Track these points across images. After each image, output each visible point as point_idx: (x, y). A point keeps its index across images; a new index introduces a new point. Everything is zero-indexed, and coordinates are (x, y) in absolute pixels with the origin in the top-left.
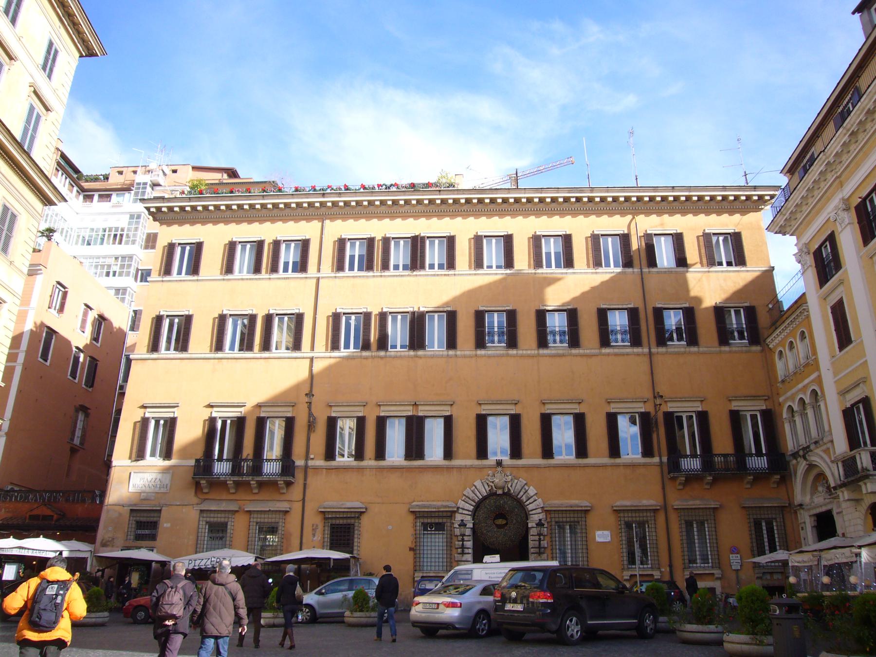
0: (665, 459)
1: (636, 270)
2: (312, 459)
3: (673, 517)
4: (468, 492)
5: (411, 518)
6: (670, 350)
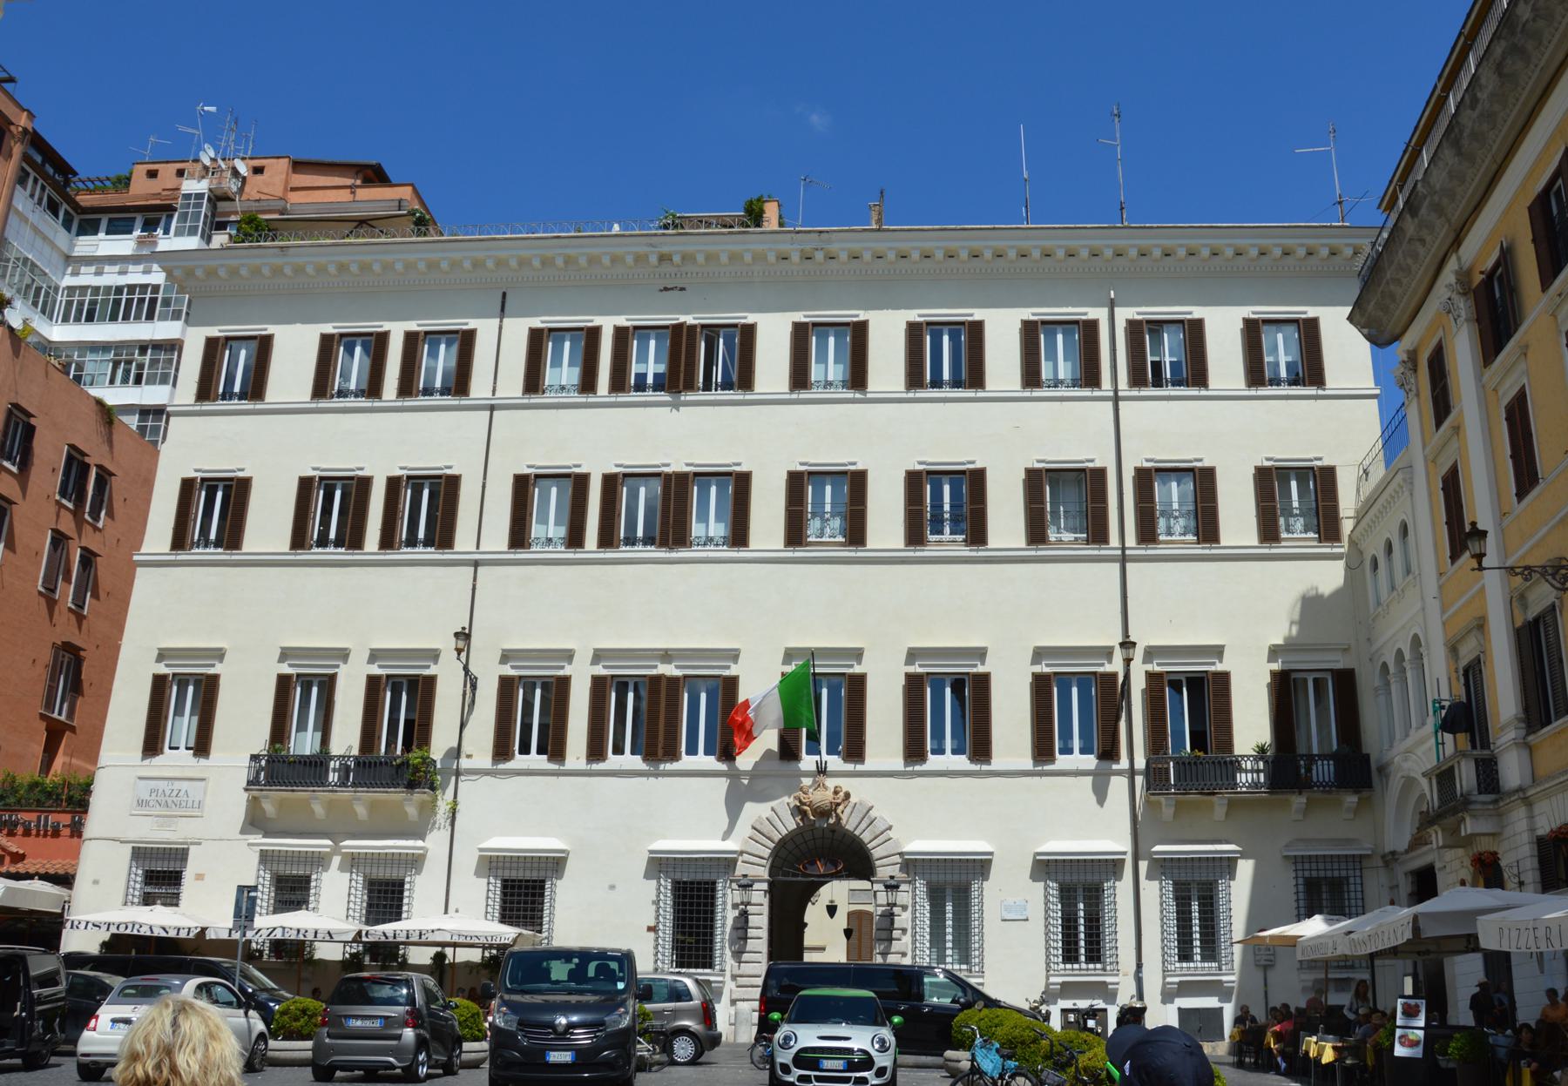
2: (469, 756)
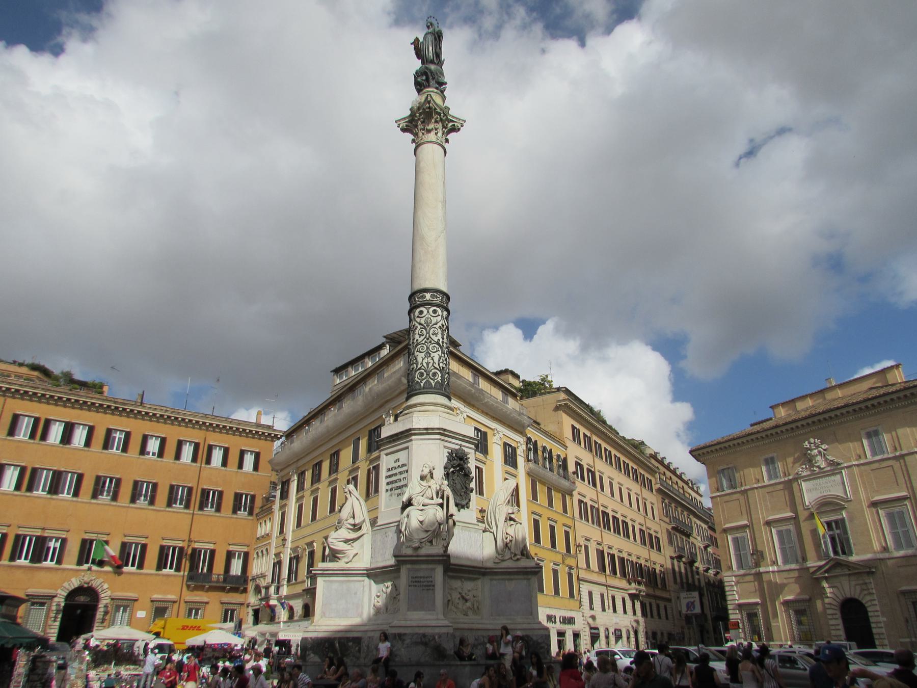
0: (186, 573)
1: (198, 465)
3: (183, 605)
4: (66, 584)
5: (150, 603)
6: (205, 513)
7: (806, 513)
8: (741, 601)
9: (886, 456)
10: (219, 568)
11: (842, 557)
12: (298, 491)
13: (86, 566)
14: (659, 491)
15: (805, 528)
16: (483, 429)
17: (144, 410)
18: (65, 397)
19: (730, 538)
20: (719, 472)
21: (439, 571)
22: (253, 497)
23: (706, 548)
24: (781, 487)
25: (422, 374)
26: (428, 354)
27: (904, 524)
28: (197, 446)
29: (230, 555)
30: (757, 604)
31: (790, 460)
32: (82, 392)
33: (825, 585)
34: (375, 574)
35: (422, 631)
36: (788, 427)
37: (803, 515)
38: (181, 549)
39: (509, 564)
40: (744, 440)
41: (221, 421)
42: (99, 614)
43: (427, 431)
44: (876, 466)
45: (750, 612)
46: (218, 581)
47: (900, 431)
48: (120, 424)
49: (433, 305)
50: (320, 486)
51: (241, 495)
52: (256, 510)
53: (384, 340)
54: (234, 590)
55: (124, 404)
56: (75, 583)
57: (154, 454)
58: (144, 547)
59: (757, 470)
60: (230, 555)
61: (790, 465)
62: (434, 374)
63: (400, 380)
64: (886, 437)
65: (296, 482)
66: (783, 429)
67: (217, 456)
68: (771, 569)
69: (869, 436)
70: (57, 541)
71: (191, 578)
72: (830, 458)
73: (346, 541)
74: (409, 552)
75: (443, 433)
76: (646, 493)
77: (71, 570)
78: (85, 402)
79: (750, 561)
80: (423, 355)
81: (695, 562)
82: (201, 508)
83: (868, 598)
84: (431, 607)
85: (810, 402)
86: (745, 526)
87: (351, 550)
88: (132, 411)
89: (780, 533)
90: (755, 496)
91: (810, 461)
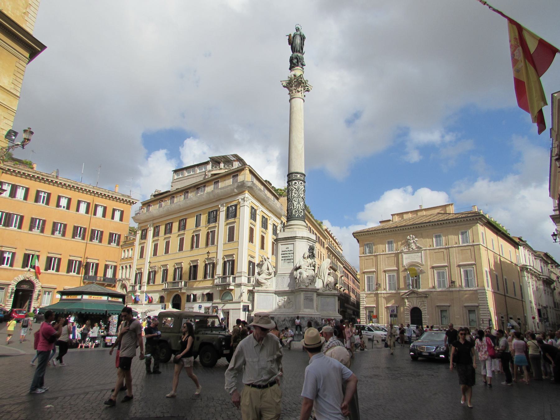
4: (16, 278)
7: (403, 269)
8: (367, 305)
9: (442, 247)
10: (100, 274)
11: (416, 289)
12: (154, 236)
13: (27, 269)
14: (327, 248)
15: (402, 275)
16: (266, 217)
17: (59, 181)
18: (12, 169)
19: (366, 276)
20: (365, 245)
21: (315, 294)
22: (120, 236)
23: (341, 277)
24: (393, 255)
25: (296, 212)
26: (299, 203)
27: (443, 277)
28: (89, 204)
29: (106, 267)
30: (374, 307)
31: (400, 243)
32: (21, 167)
33: (406, 301)
34: (278, 293)
35: (310, 316)
36: (402, 228)
37: (401, 269)
38: (80, 262)
39: (328, 292)
40: (380, 231)
41: (103, 191)
42: (35, 296)
43: (302, 238)
44: (437, 251)
45: (370, 310)
46: (100, 281)
47: (450, 237)
48: (45, 188)
49: (301, 180)
50: (171, 236)
51: (113, 234)
52: (121, 243)
53: (209, 159)
54: (109, 285)
55: (47, 176)
56: (21, 278)
57: (64, 207)
58: (60, 260)
59: (383, 246)
60: (106, 267)
61: (399, 246)
62: (301, 212)
63: (234, 190)
64: (443, 238)
65: (152, 232)
66: (399, 229)
67: (100, 211)
68: (383, 292)
69: (436, 237)
70: (9, 254)
71: (85, 278)
72: (418, 245)
73: (266, 279)
74: (304, 287)
75: (308, 239)
76: (322, 249)
77: (18, 270)
78: (24, 173)
79: (374, 287)
80: (297, 203)
81: (337, 284)
82: (91, 240)
83: (423, 307)
84: (312, 308)
85: (410, 215)
86: (374, 272)
87: (268, 283)
88: (52, 181)
89: (389, 276)
90: (381, 258)
91: (409, 245)
